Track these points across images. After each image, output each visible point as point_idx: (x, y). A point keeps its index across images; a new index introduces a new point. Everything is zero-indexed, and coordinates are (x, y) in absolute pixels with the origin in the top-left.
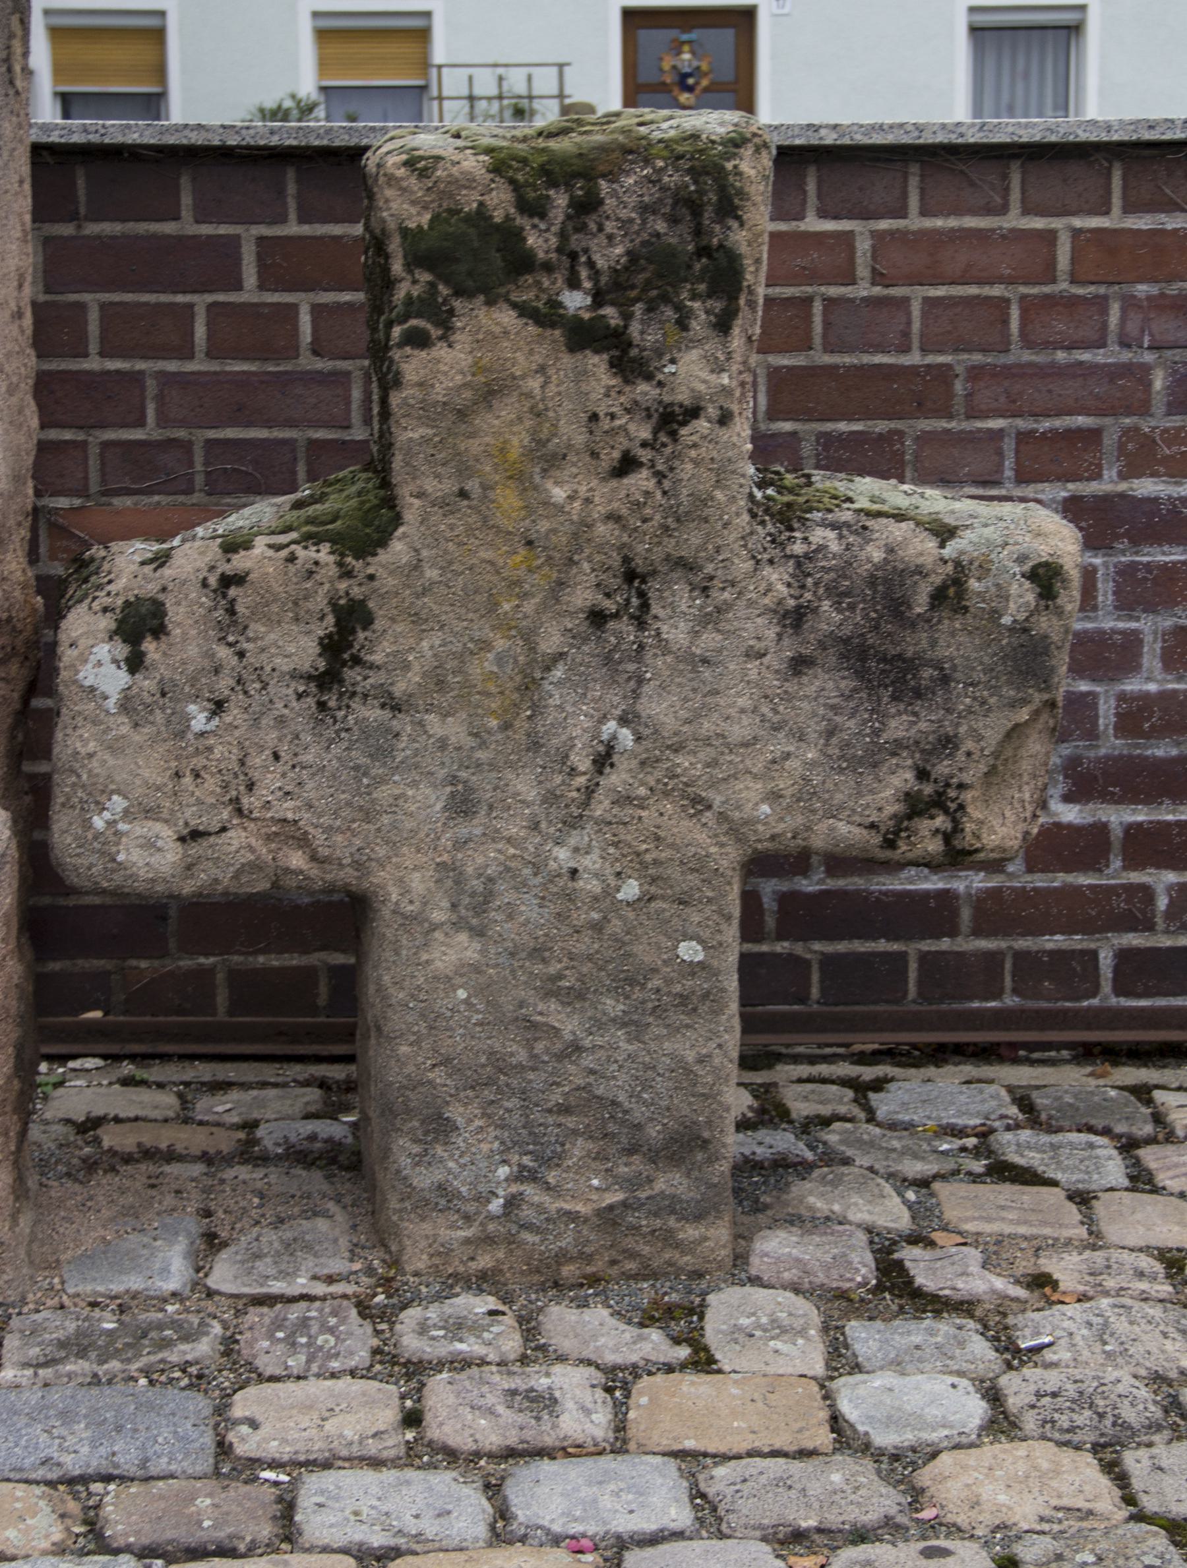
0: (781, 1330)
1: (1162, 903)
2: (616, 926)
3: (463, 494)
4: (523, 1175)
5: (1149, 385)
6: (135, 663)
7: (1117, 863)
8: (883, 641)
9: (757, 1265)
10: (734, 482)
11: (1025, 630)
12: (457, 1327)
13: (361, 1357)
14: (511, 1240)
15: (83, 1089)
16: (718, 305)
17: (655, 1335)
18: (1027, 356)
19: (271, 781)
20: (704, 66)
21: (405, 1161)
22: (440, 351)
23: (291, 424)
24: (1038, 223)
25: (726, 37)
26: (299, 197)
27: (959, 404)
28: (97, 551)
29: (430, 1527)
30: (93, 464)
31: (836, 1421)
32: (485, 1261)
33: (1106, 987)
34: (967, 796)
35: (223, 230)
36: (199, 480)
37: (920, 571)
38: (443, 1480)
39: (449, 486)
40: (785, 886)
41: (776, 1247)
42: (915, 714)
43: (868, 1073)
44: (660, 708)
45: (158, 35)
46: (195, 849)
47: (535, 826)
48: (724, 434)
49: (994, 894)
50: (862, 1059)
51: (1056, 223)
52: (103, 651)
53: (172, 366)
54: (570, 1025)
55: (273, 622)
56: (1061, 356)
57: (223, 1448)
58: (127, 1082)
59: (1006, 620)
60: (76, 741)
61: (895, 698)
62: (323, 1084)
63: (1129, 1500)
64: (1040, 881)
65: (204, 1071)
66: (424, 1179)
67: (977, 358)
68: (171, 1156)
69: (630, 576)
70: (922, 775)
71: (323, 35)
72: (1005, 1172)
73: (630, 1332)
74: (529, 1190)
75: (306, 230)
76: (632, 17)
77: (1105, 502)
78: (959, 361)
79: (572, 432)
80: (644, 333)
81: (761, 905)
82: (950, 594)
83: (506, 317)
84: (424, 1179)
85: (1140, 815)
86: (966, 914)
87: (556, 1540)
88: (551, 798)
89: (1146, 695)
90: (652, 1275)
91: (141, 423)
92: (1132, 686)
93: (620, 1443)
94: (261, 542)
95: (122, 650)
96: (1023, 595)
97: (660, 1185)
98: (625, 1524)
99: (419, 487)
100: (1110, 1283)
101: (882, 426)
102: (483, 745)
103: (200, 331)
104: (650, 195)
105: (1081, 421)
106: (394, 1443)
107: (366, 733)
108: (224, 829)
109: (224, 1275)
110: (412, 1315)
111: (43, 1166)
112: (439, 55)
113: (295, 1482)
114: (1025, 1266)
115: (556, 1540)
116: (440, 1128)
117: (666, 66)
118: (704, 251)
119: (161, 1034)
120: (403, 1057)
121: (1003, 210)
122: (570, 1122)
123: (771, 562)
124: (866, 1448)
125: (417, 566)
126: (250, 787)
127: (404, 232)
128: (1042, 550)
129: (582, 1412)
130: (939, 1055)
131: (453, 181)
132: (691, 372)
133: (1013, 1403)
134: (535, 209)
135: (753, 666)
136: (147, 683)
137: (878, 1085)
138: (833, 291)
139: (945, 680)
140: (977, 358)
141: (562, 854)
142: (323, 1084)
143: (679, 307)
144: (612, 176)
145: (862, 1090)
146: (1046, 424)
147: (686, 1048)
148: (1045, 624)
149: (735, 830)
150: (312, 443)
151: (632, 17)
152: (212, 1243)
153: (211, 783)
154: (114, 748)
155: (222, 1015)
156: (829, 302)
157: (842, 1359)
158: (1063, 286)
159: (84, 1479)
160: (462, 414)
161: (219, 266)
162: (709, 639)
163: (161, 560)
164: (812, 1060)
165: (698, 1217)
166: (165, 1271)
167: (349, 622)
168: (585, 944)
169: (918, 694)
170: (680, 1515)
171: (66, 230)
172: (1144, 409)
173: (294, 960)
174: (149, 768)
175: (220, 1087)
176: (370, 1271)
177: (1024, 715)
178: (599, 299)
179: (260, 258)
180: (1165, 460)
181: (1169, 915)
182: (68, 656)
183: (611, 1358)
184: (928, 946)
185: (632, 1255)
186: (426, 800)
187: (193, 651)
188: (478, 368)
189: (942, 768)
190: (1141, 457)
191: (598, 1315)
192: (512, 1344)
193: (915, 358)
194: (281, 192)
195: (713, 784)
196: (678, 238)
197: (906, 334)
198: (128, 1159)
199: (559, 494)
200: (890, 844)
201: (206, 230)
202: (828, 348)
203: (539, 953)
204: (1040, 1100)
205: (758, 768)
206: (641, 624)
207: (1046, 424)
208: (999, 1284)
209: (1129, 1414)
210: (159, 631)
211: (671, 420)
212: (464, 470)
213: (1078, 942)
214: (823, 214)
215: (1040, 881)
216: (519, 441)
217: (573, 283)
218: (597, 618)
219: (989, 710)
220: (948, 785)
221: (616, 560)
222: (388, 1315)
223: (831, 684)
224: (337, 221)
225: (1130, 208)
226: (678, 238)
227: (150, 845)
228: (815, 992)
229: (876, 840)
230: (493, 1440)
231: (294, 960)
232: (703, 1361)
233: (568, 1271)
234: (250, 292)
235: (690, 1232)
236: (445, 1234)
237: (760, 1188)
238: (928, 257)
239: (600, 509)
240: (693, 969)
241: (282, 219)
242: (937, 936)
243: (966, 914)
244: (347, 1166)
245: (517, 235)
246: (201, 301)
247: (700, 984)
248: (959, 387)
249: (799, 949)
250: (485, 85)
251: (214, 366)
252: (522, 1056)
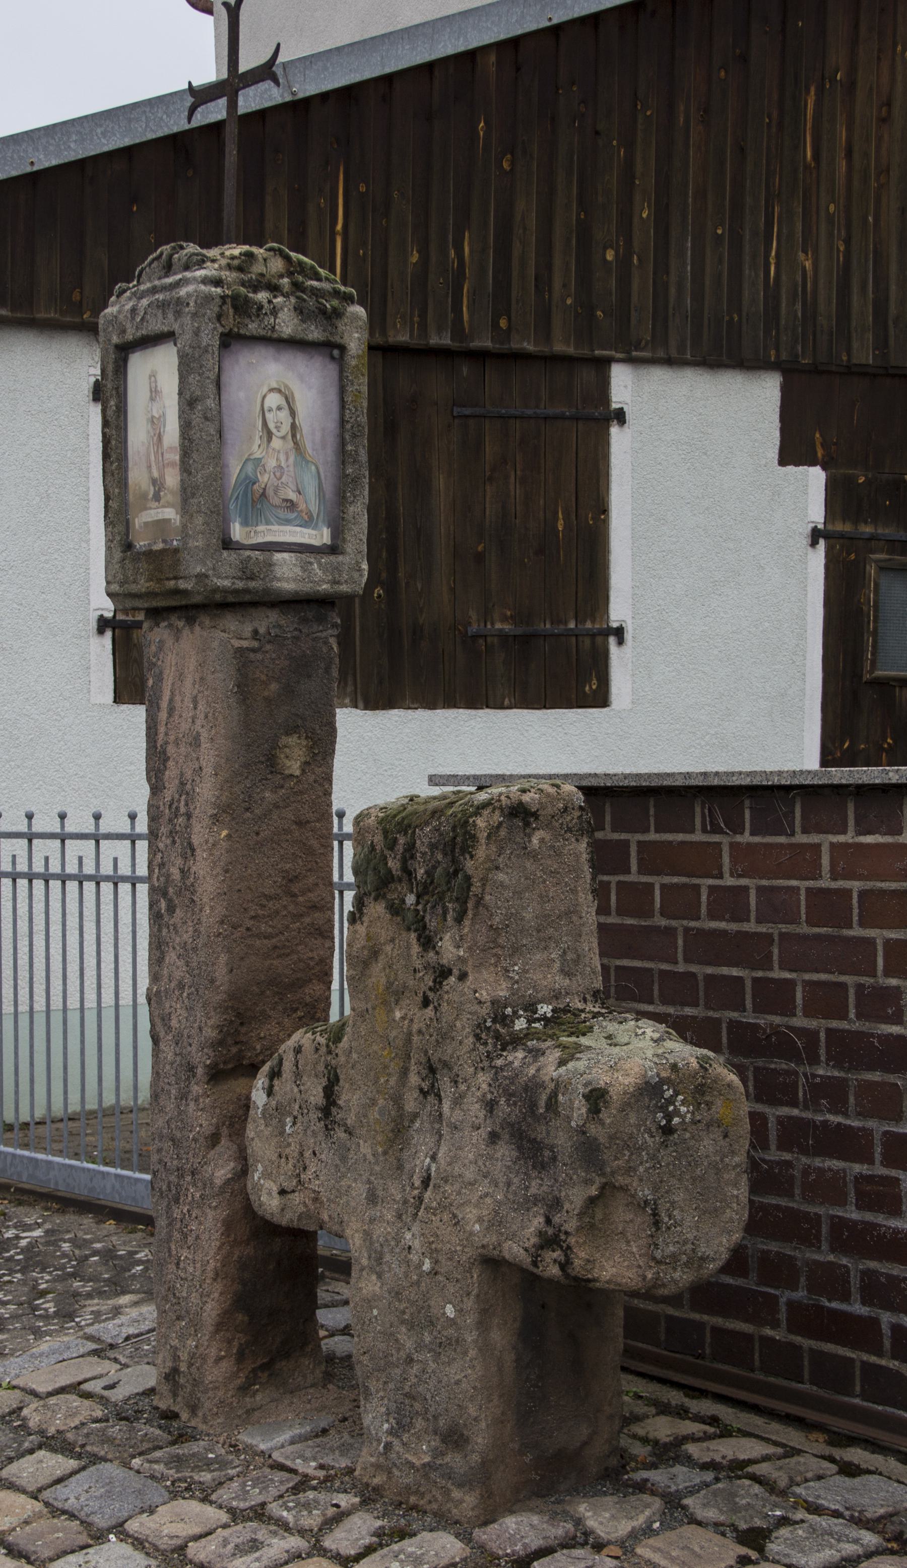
11: (584, 1133)
26: (656, 816)
42: (542, 1179)
48: (460, 986)
59: (573, 1124)
61: (534, 1167)
70: (548, 1221)
81: (881, 1330)
96: (580, 1109)
108: (293, 1191)
123: (483, 1069)
126: (305, 1169)
148: (593, 1130)
219: (574, 1184)
220: (560, 1231)
223: (507, 1153)
224: (671, 831)
235: (456, 1494)
240: (452, 1322)
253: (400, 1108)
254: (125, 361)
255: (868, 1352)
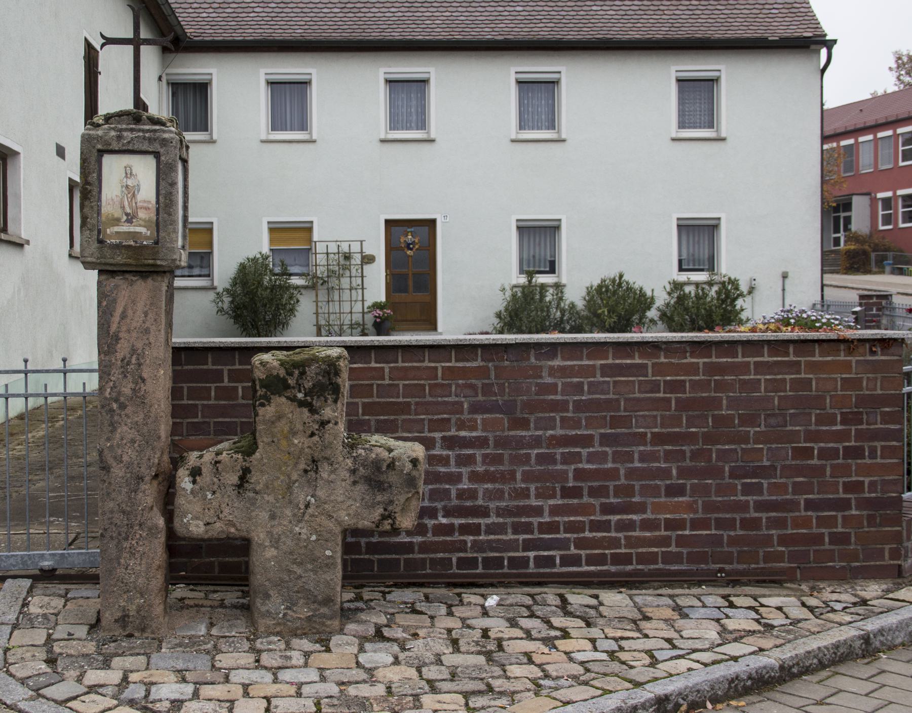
0: (348, 644)
1: (469, 545)
2: (310, 547)
3: (273, 442)
4: (287, 608)
5: (463, 407)
6: (194, 482)
7: (457, 534)
8: (375, 476)
9: (345, 631)
10: (338, 439)
12: (270, 643)
13: (247, 648)
14: (285, 624)
15: (180, 591)
16: (334, 397)
17: (318, 645)
18: (431, 399)
19: (226, 511)
20: (417, 241)
21: (259, 605)
22: (268, 408)
23: (236, 417)
24: (433, 365)
25: (426, 229)
27: (413, 412)
28: (185, 454)
29: (259, 680)
30: (185, 428)
31: (357, 663)
32: (278, 629)
33: (455, 568)
34: (396, 515)
35: (219, 367)
36: (212, 432)
37: (384, 460)
38: (263, 672)
39: (270, 440)
40: (367, 540)
41: (351, 627)
43: (387, 590)
44: (321, 493)
45: (210, 231)
46: (208, 527)
47: (290, 522)
48: (336, 427)
49: (425, 542)
50: (387, 587)
51: (437, 365)
52: (187, 479)
53: (205, 402)
54: (299, 571)
55: (227, 472)
56: (439, 399)
57: (213, 666)
58: (191, 590)
60: (180, 501)
62: (242, 591)
63: (421, 676)
64: (436, 539)
65: (212, 588)
66: (263, 609)
67: (417, 400)
68: (202, 606)
69: (314, 461)
70: (385, 510)
71: (272, 230)
72: (415, 611)
73: (311, 644)
74: (289, 612)
75: (241, 367)
76: (388, 223)
77: (452, 438)
78: (412, 400)
79: (299, 427)
80: (316, 403)
82: (391, 465)
83: (284, 399)
84: (263, 609)
85: (463, 521)
86: (416, 548)
87: (288, 683)
88: (294, 515)
89: (464, 489)
90: (319, 633)
91: (197, 417)
92: (460, 486)
93: (306, 665)
94: (225, 453)
95: (191, 479)
96: (409, 466)
97: (321, 611)
98: (303, 680)
99: (263, 440)
100: (432, 635)
101: (392, 417)
102: (278, 502)
103: (213, 394)
104: (318, 371)
105: (445, 416)
106: (253, 665)
107: (249, 499)
109: (214, 632)
110: (259, 640)
111: (171, 607)
112: (316, 237)
113: (229, 673)
114: (412, 632)
115: (288, 683)
116: (267, 596)
117: (402, 241)
118: (331, 384)
119: (200, 578)
120: (258, 579)
121: (423, 361)
122: (299, 595)
124: (363, 667)
125: (262, 459)
127: (260, 379)
128: (414, 455)
129: (297, 658)
130: (408, 585)
131: (271, 368)
132: (327, 413)
133: (400, 659)
134: (290, 374)
135: (343, 484)
136: (197, 487)
137: (389, 593)
138: (379, 382)
139: (390, 486)
140: (417, 400)
141: (297, 529)
142: (242, 591)
143: (325, 397)
144: (309, 366)
145: (384, 593)
146: (436, 417)
147: (328, 577)
148: (414, 473)
149: (339, 523)
150: (242, 422)
151: (388, 223)
152: (212, 625)
153: (212, 511)
154: (189, 502)
155: (216, 574)
156: (378, 385)
157: (362, 649)
158: (440, 381)
159: (182, 671)
160: (273, 423)
161: (218, 376)
162: (333, 476)
163: (201, 457)
164: (374, 587)
165: (331, 619)
166: (200, 630)
167: (245, 473)
168: (303, 551)
169: (384, 490)
170: (317, 679)
171: (179, 368)
172: (462, 413)
173: (236, 559)
174: (197, 508)
175: (215, 592)
176: (250, 631)
177: (410, 495)
178: (306, 395)
179: (229, 375)
180: (468, 426)
181: (471, 548)
182: (178, 480)
183: (306, 650)
184: (406, 556)
185: (315, 628)
186: (264, 515)
187: (208, 479)
188: (277, 412)
189: (390, 508)
190: (461, 426)
191: (305, 641)
192: (283, 646)
193: (401, 400)
194: (234, 357)
195: (334, 512)
196: (325, 380)
197: (398, 393)
198: (191, 607)
199: (296, 441)
200: (378, 527)
201: (215, 367)
202: (378, 397)
203: (291, 553)
204: (431, 596)
205: (345, 508)
206: (317, 473)
207: (436, 417)
208: (404, 635)
209: (427, 661)
210: (200, 474)
211: (323, 424)
212: (273, 436)
213: (447, 555)
214: (376, 362)
215: (436, 539)
216: (286, 429)
217: (300, 391)
218: (306, 471)
221: (310, 457)
222: (254, 640)
225: (456, 361)
226: (325, 380)
227: (197, 526)
228: (376, 569)
229: (374, 526)
230: (275, 664)
231: (236, 559)
232: (328, 650)
233: (299, 632)
234: (226, 383)
235: (329, 622)
236: (268, 622)
237: (347, 614)
238: (404, 373)
239: (306, 445)
240: (329, 557)
241: (234, 364)
242: (409, 554)
243: (416, 548)
244: (246, 609)
245: (286, 380)
246: (213, 386)
247: (331, 561)
248: (413, 407)
249: (371, 557)
250: (333, 248)
251: (216, 402)
252: (287, 579)
253: (290, 478)
254: (102, 156)
255: (355, 554)
